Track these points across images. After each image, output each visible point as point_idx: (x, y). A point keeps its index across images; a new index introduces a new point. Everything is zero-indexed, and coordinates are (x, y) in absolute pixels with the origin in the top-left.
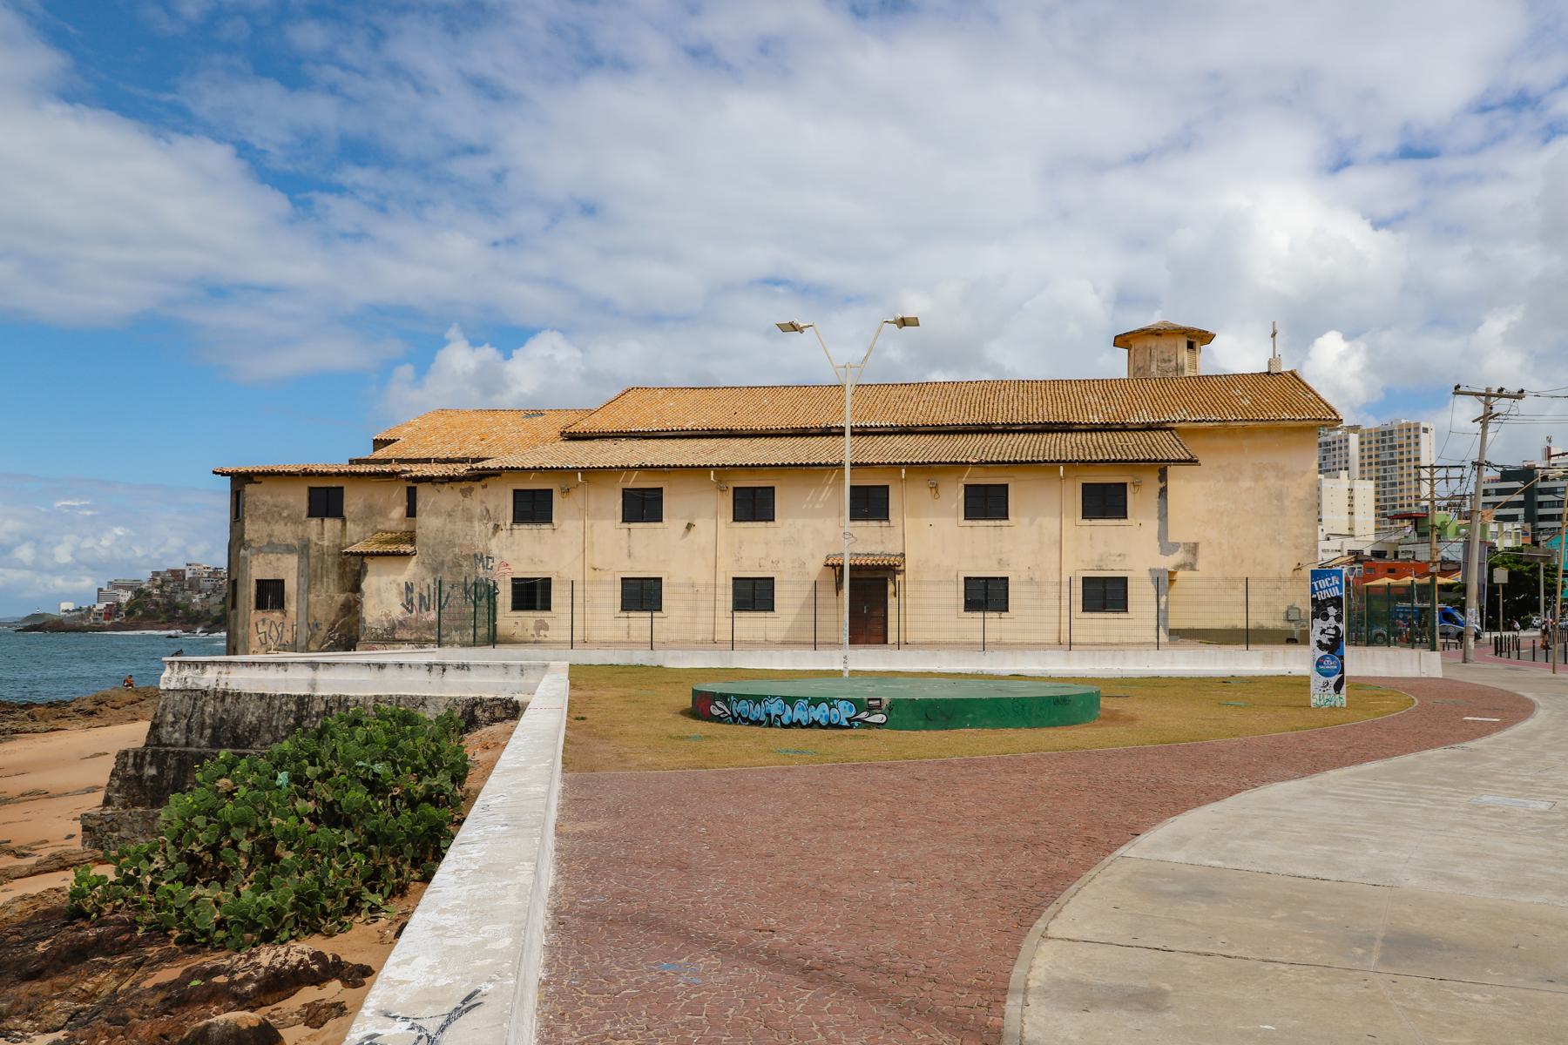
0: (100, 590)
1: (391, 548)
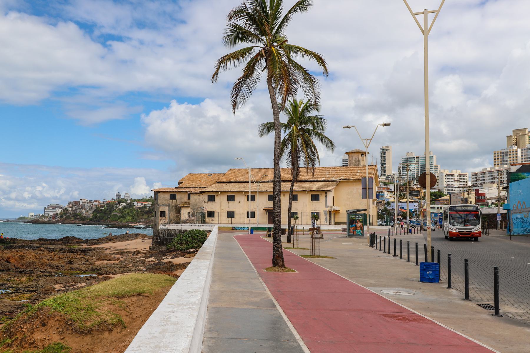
0: (45, 208)
1: (186, 206)
